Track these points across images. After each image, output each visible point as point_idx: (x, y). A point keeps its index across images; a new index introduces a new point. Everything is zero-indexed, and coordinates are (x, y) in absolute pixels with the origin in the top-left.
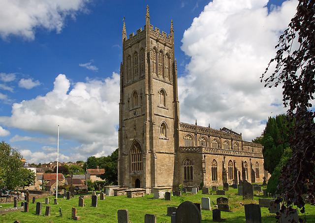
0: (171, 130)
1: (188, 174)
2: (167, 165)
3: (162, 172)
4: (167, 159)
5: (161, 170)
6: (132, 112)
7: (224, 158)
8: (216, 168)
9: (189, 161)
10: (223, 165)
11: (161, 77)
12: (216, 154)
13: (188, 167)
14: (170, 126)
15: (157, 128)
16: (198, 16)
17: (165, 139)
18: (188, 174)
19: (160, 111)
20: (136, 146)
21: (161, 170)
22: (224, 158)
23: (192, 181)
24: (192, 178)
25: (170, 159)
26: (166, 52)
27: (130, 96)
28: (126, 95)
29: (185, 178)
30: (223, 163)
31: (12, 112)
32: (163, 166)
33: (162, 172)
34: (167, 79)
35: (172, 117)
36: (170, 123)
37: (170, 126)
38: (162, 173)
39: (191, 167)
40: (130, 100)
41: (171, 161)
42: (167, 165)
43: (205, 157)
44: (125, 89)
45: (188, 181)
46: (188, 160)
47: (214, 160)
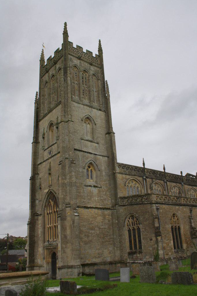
0: (104, 173)
1: (135, 240)
2: (100, 228)
3: (90, 238)
4: (100, 219)
5: (88, 236)
6: (47, 151)
7: (191, 211)
8: (179, 228)
9: (135, 219)
10: (191, 223)
11: (86, 102)
12: (177, 205)
13: (134, 229)
14: (103, 168)
15: (81, 170)
16: (62, 44)
17: (95, 186)
18: (135, 240)
19: (86, 146)
20: (52, 200)
21: (88, 236)
22: (191, 211)
23: (140, 252)
24: (140, 247)
25: (104, 218)
26: (92, 73)
27: (45, 132)
28: (41, 130)
29: (131, 248)
30: (190, 219)
31: (14, 292)
32: (92, 229)
33: (90, 238)
34: (95, 104)
35: (105, 154)
36: (103, 162)
37: (103, 168)
38: (91, 241)
39: (139, 229)
40: (46, 136)
41: (107, 221)
42: (100, 228)
43: (157, 209)
44: (41, 123)
45: (135, 253)
46: (132, 217)
47: (174, 215)
